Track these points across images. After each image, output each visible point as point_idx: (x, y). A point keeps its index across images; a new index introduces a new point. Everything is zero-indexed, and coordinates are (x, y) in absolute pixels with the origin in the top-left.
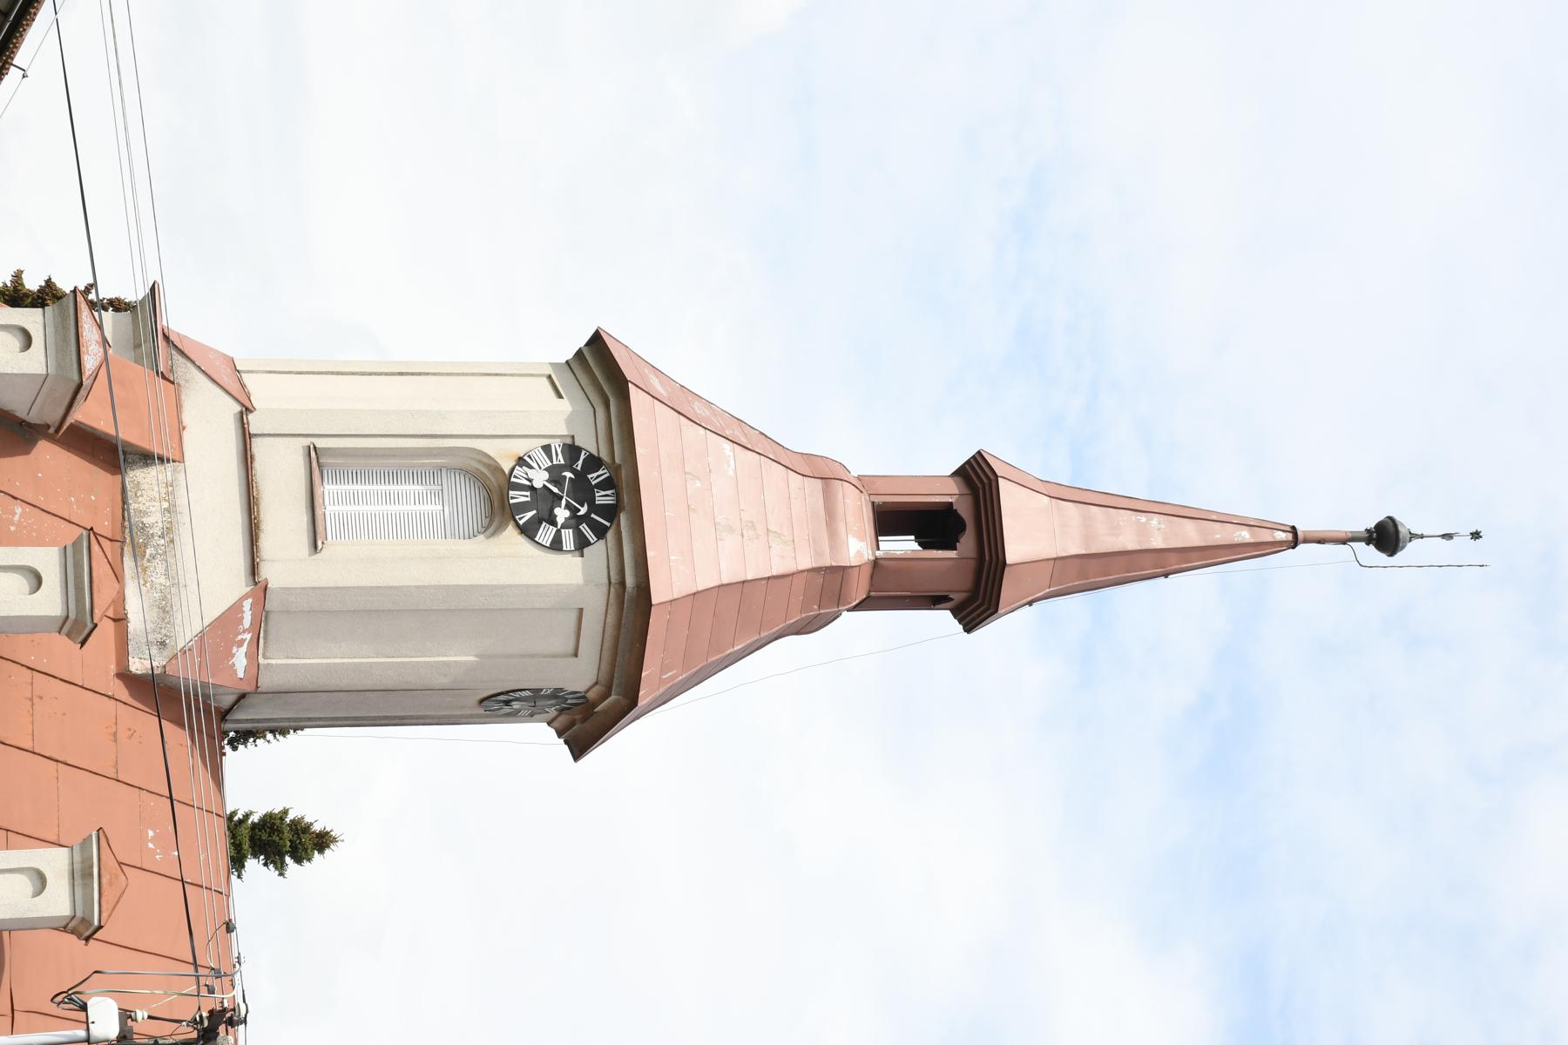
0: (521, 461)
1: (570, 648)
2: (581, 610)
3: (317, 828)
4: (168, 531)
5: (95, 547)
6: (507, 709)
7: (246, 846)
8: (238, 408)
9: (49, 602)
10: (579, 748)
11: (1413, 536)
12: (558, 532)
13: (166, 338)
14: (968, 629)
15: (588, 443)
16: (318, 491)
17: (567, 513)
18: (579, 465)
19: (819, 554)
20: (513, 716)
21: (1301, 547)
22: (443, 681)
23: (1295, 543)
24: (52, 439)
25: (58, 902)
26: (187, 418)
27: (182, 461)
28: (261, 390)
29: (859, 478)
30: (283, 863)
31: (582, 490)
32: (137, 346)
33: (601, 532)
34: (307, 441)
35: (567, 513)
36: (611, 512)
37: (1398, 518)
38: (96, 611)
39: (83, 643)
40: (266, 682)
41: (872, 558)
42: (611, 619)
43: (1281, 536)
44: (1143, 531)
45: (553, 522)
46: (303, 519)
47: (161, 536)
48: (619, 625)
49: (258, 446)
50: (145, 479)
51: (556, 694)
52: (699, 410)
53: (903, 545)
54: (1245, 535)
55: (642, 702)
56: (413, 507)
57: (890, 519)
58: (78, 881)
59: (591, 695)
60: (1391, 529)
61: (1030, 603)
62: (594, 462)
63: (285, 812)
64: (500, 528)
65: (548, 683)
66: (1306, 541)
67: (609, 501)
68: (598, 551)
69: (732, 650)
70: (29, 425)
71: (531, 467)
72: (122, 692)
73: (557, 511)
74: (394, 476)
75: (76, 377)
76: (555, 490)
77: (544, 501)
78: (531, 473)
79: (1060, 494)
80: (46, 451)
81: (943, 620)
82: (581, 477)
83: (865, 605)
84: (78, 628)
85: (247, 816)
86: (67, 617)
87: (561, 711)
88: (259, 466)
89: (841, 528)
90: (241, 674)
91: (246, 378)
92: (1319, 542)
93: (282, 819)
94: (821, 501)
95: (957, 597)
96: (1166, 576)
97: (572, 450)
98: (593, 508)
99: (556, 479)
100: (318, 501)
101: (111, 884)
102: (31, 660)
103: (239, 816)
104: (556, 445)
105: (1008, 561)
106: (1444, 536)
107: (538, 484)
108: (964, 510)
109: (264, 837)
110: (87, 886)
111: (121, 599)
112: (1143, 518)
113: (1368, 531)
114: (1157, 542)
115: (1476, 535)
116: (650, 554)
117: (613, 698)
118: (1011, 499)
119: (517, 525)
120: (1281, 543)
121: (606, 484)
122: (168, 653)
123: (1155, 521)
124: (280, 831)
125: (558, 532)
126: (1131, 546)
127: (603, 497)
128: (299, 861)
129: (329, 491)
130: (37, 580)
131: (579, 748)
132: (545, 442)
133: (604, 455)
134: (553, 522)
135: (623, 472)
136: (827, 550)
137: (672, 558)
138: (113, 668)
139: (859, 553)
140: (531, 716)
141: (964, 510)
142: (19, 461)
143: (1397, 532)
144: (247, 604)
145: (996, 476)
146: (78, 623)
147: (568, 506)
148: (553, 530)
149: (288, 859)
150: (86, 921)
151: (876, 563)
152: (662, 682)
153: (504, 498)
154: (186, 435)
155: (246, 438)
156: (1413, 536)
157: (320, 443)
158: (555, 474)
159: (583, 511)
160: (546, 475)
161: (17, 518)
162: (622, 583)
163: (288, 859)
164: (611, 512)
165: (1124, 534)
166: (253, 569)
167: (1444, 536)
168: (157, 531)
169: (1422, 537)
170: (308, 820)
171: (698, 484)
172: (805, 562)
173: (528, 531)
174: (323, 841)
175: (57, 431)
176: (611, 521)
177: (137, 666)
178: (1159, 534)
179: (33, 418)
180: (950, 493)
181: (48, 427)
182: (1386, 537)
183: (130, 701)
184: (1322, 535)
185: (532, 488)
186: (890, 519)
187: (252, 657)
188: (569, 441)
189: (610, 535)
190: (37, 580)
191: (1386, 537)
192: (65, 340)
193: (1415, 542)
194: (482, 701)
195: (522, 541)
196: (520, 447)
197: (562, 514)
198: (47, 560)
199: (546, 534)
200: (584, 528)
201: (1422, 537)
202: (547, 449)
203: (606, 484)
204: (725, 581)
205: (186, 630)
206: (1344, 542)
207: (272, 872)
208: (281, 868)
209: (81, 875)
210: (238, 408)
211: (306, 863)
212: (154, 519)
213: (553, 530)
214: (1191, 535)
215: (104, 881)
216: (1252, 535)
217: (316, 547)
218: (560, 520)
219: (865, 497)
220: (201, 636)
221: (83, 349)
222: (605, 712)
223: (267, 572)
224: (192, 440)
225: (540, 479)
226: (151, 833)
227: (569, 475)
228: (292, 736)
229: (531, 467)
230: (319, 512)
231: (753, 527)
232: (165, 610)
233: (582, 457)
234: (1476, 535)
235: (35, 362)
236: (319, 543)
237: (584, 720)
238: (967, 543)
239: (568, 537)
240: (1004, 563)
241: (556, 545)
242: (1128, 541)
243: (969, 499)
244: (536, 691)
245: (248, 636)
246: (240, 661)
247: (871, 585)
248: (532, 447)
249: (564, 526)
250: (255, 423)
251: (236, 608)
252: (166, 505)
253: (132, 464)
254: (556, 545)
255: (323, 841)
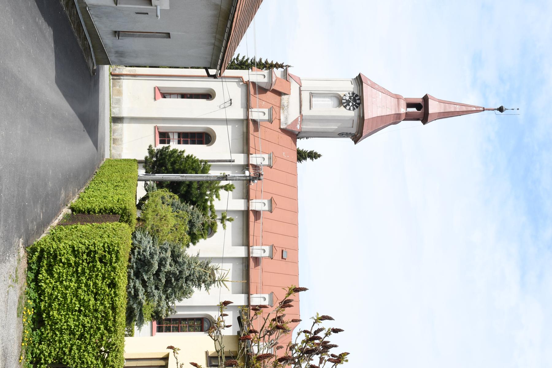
0: (345, 95)
1: (352, 126)
2: (353, 120)
3: (318, 153)
4: (287, 106)
5: (273, 109)
6: (342, 136)
7: (307, 156)
8: (299, 86)
9: (266, 117)
10: (356, 143)
11: (506, 109)
12: (350, 107)
13: (289, 75)
14: (424, 124)
15: (356, 92)
16: (311, 100)
17: (352, 104)
18: (354, 96)
19: (396, 111)
20: (344, 137)
21: (485, 111)
22: (332, 131)
23: (484, 110)
24: (269, 91)
25: (266, 162)
26: (291, 88)
27: (290, 94)
28: (304, 83)
29: (405, 98)
30: (313, 159)
31: (355, 100)
32: (284, 76)
33: (357, 107)
34: (310, 92)
35: (352, 104)
36: (359, 104)
37: (503, 106)
38: (273, 119)
39: (271, 123)
40: (303, 130)
41: (405, 112)
42: (358, 122)
43: (481, 109)
44: (455, 108)
45: (349, 106)
46: (309, 104)
47: (286, 107)
48: (360, 123)
49: (302, 92)
50: (283, 97)
51: (350, 133)
52: (376, 86)
53: (414, 110)
54: (474, 109)
55: (364, 135)
56: (326, 102)
57: (409, 105)
58: (269, 159)
59: (356, 134)
60: (502, 108)
61: (435, 120)
62: (357, 96)
63: (303, 150)
64: (341, 106)
65: (349, 132)
66: (486, 110)
67: (359, 102)
68: (357, 110)
69: (380, 127)
70: (266, 89)
71: (346, 96)
72: (280, 131)
73: (350, 104)
74: (324, 97)
75: (271, 82)
76: (350, 100)
77: (348, 102)
78: (346, 97)
79: (440, 101)
80: (269, 93)
81: (420, 122)
82: (354, 98)
83: (405, 120)
84: (270, 121)
85: (307, 151)
86: (269, 120)
87: (352, 136)
88: (302, 96)
89: (400, 107)
90: (298, 129)
91: (302, 81)
92: (488, 110)
93: (313, 152)
94: (397, 103)
95: (421, 119)
96: (460, 116)
97: (353, 94)
98: (356, 103)
99: (350, 98)
100: (311, 101)
101: (274, 160)
102: (265, 126)
103: (306, 151)
104: (351, 93)
105: (429, 113)
106: (512, 109)
107: (347, 99)
108: (423, 104)
109: (310, 154)
110: (271, 160)
111: (280, 116)
112: (455, 106)
113: (498, 108)
114: (458, 110)
115: (518, 109)
116: (365, 111)
117: (359, 134)
118: (430, 102)
119: (343, 106)
120: (481, 110)
121: (359, 99)
122: (287, 125)
123: (458, 106)
124: (312, 154)
125: (350, 107)
126: (453, 111)
127: (358, 101)
128: (315, 159)
129: (314, 100)
130: (265, 114)
131: (356, 143)
132: (349, 92)
133: (359, 95)
134: (349, 106)
135: (361, 97)
136: (397, 111)
137: (369, 112)
138: (278, 127)
139: (403, 111)
140: (347, 137)
141: (423, 104)
142: (264, 95)
143: (503, 109)
144: (299, 118)
145: (428, 98)
146: (270, 120)
147: (352, 103)
148: (349, 107)
149: (314, 158)
150: (270, 165)
151: (406, 113)
152: (367, 132)
153: (342, 101)
154: (291, 90)
155: (300, 91)
156: (506, 109)
157: (312, 92)
158: (350, 97)
159: (354, 104)
160: (349, 98)
161: (263, 104)
162: (360, 116)
163: (314, 158)
164: (359, 104)
165: (452, 109)
166: (300, 112)
167: (512, 109)
168: (286, 106)
169: (508, 109)
170: (317, 152)
171: (374, 99)
172: (393, 113)
173: (345, 107)
174: (319, 156)
175: (270, 90)
176: (359, 105)
177: (282, 127)
178: (458, 108)
179: (266, 88)
180: (420, 101)
181: (268, 90)
182: (501, 109)
183: (281, 132)
184: (489, 109)
185: (346, 100)
186: (409, 105)
187: (300, 126)
188: (353, 92)
189: (359, 108)
190: (265, 114)
191: (501, 109)
192: (270, 77)
193: (506, 110)
194: (338, 134)
195: (344, 108)
196: (345, 93)
197: (351, 104)
198: (266, 111)
199: (348, 107)
200: (354, 106)
201: (508, 109)
202: (349, 93)
203: (359, 99)
204: (378, 116)
205: (290, 122)
206: (493, 110)
207: (311, 160)
208: (313, 160)
209: (270, 158)
210: (299, 86)
211: (317, 159)
212: (286, 104)
213: (349, 107)
214: (464, 109)
215: (273, 160)
216: (476, 109)
217: (310, 109)
218: (350, 105)
219: (405, 102)
220: (292, 123)
221: (273, 78)
222: (358, 137)
223: (302, 113)
224: (292, 91)
225: (348, 98)
226: (284, 153)
227: (352, 98)
228: (309, 139)
229: (346, 96)
230: (311, 103)
231: (384, 107)
232: (286, 118)
233: (355, 94)
234: (518, 109)
235: (266, 80)
236: (311, 108)
237: (355, 138)
238: (422, 111)
239: (352, 108)
240: (429, 114)
241: (350, 109)
242: (452, 110)
243: (424, 102)
244: (347, 133)
245: (300, 123)
246: (298, 127)
247: (406, 116)
248: (347, 93)
249: (351, 106)
250: (302, 88)
251: (298, 118)
252: (287, 102)
253: (283, 95)
254: (350, 109)
255: (319, 156)
